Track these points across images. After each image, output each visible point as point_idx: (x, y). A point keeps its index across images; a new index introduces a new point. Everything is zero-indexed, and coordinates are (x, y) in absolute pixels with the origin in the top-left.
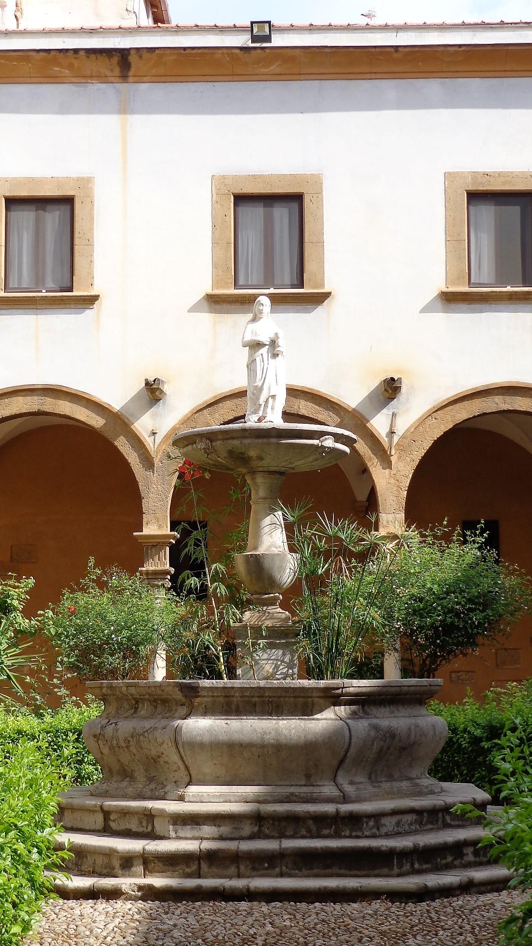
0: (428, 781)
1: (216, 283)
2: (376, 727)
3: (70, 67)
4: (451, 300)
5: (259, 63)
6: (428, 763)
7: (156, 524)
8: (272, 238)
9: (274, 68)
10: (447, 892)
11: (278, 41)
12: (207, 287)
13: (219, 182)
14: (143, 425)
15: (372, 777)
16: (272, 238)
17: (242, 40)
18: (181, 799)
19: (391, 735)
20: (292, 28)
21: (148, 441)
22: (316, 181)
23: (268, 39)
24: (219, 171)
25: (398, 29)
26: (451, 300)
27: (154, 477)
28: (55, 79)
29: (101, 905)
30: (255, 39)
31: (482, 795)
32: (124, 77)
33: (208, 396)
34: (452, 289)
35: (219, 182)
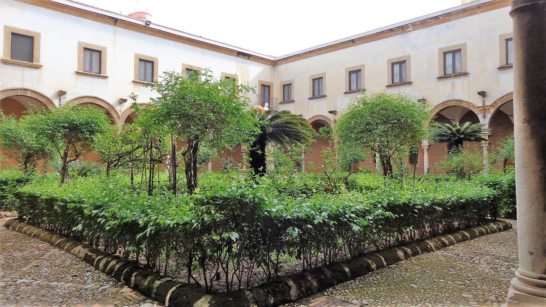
1: (78, 68)
3: (102, 18)
4: (134, 82)
5: (146, 29)
8: (93, 61)
9: (149, 32)
11: (151, 26)
12: (133, 79)
13: (136, 55)
14: (118, 108)
16: (93, 61)
17: (143, 24)
20: (155, 24)
21: (119, 113)
23: (149, 25)
24: (136, 53)
25: (90, 6)
26: (77, 73)
27: (120, 121)
28: (97, 21)
30: (146, 24)
32: (115, 25)
33: (4, 88)
34: (5, 58)
35: (136, 55)
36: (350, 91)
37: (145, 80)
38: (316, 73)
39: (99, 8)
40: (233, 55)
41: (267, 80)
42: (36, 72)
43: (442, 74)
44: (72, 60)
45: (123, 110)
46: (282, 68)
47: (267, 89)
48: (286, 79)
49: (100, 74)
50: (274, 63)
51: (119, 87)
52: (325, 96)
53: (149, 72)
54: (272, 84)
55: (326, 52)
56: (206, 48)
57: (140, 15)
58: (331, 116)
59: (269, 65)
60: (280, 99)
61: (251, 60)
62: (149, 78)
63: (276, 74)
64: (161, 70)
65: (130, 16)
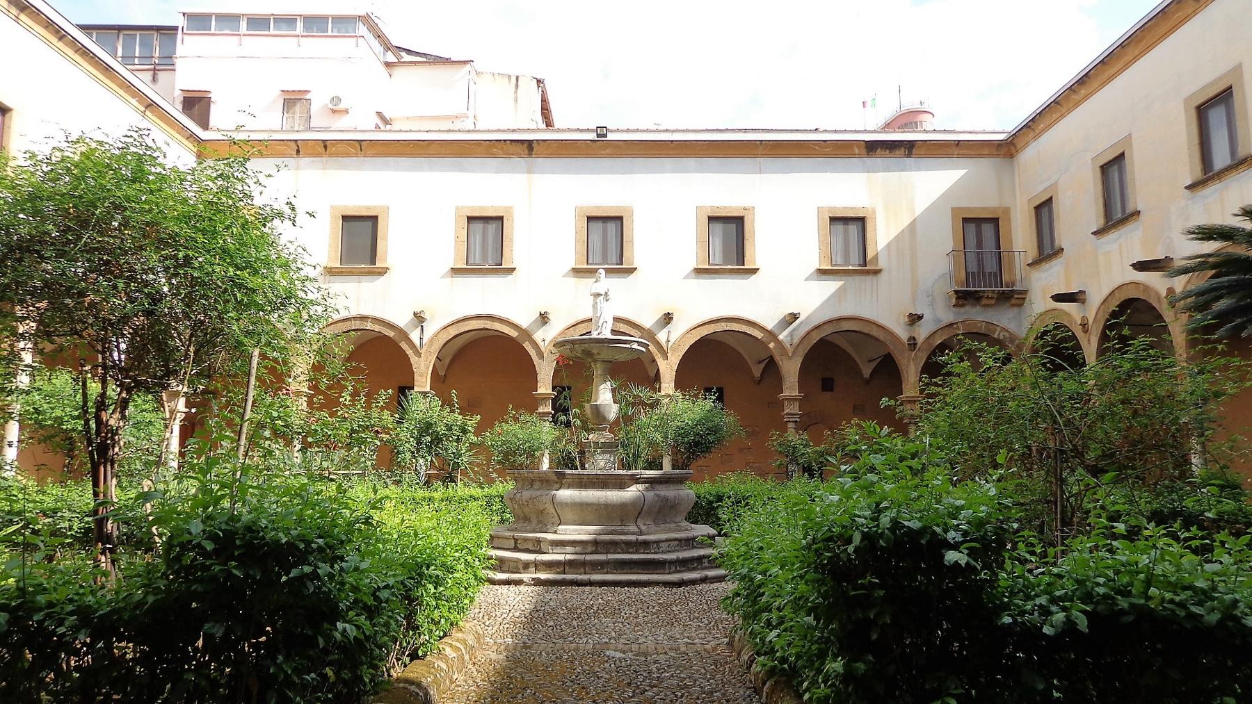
0: (685, 524)
2: (658, 495)
5: (600, 147)
6: (685, 514)
7: (545, 387)
8: (730, 238)
10: (693, 582)
11: (610, 137)
12: (693, 264)
15: (655, 522)
16: (730, 238)
17: (593, 136)
18: (555, 532)
19: (666, 499)
21: (541, 344)
22: (630, 211)
23: (605, 136)
28: (494, 156)
29: (512, 588)
31: (713, 532)
32: (530, 155)
36: (1208, 175)
37: (847, 263)
38: (1104, 147)
39: (631, 128)
40: (853, 155)
41: (983, 201)
42: (382, 280)
43: (1198, 174)
44: (446, 244)
45: (678, 338)
46: (1029, 154)
47: (988, 230)
48: (1038, 192)
49: (499, 267)
50: (1005, 149)
51: (786, 291)
52: (1137, 213)
53: (989, 244)
54: (1007, 211)
55: (1127, 66)
56: (764, 155)
57: (908, 119)
58: (1152, 279)
59: (990, 155)
60: (1032, 253)
61: (920, 156)
62: (613, 257)
63: (1017, 180)
64: (882, 236)
65: (888, 126)
